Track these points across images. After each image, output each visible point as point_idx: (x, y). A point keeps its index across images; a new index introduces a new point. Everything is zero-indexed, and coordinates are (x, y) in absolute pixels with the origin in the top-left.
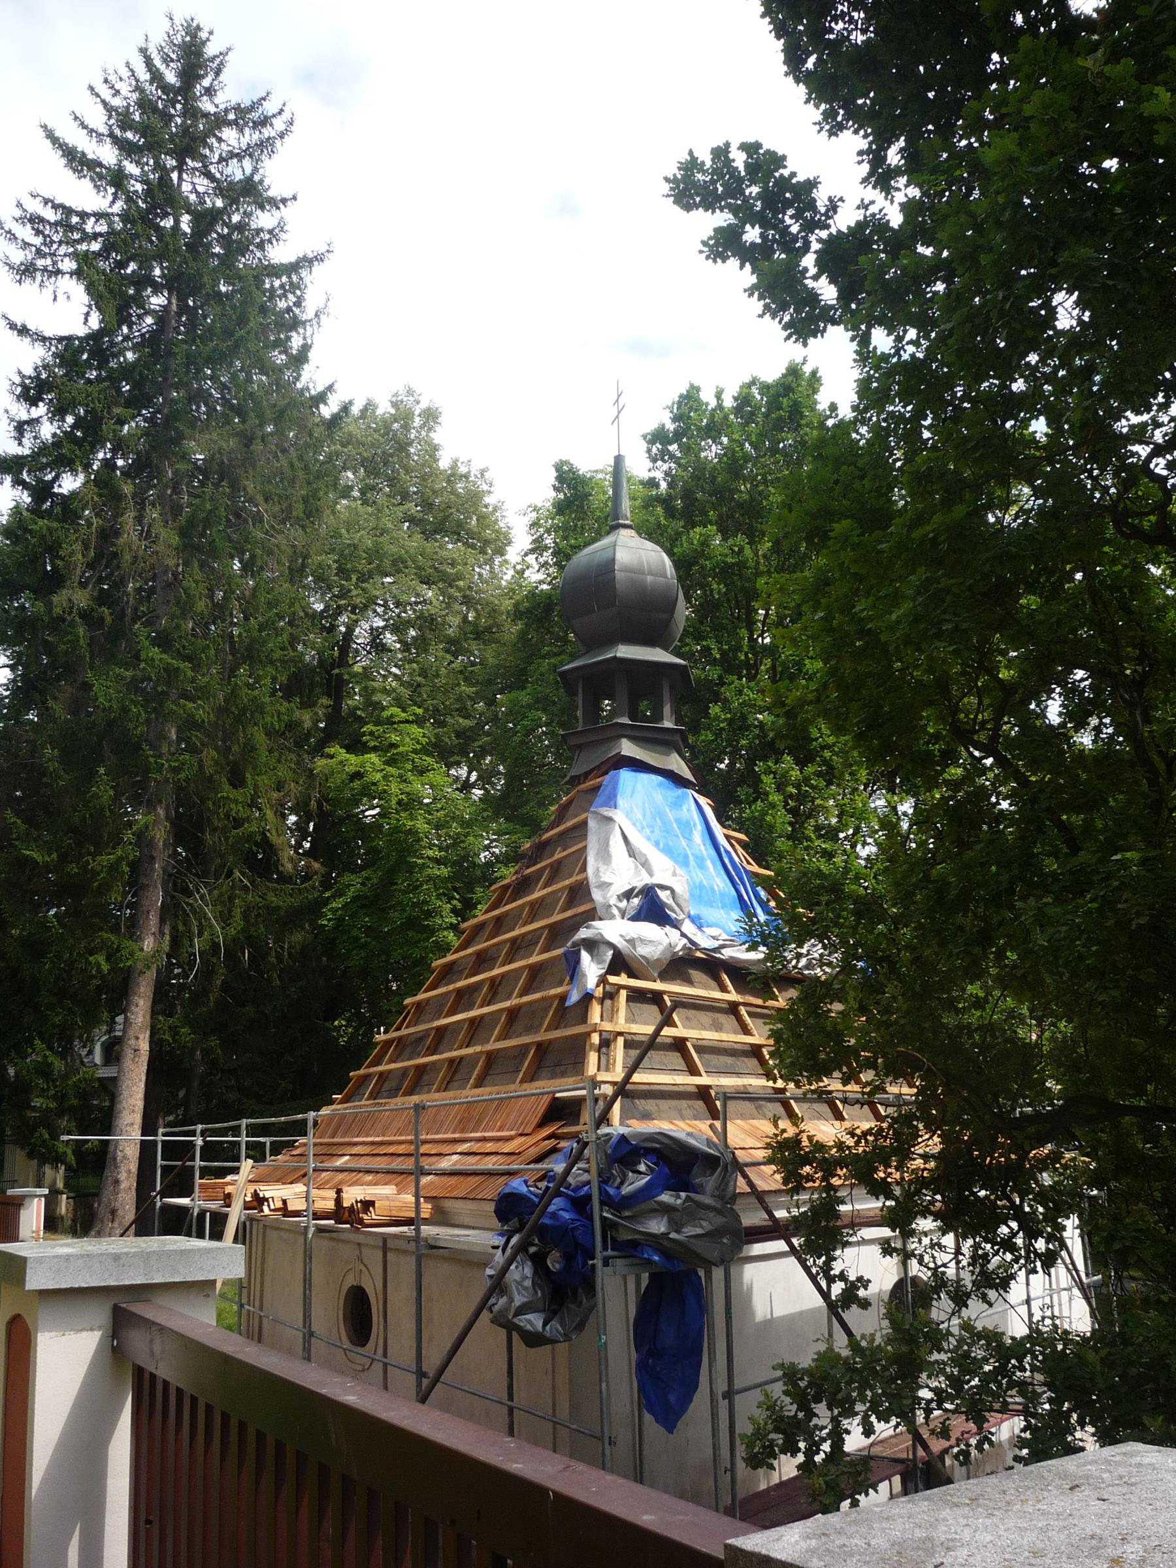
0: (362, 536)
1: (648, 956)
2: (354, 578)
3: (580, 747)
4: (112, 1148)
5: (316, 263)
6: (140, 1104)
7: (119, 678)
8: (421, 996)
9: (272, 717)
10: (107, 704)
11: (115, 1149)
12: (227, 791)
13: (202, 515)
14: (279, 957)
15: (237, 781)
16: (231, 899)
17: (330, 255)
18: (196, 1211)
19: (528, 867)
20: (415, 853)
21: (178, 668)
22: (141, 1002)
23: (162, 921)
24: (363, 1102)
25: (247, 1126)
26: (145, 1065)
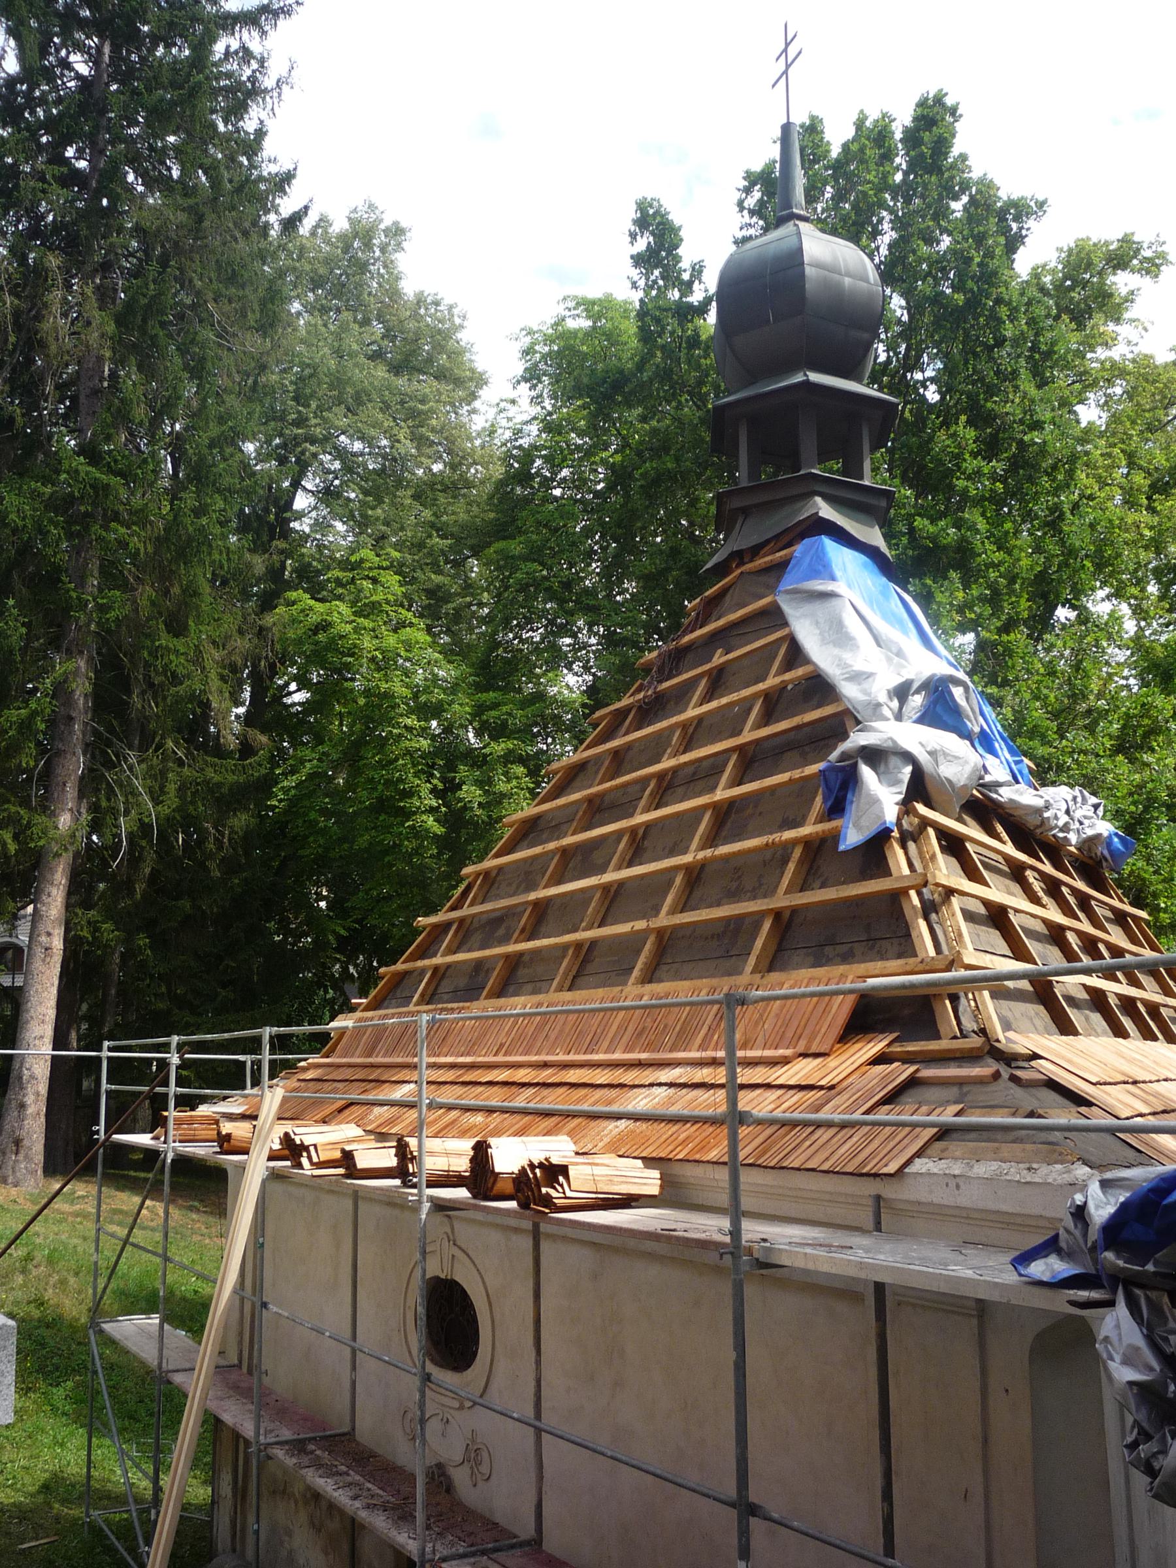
0: (324, 355)
1: (954, 780)
2: (314, 405)
3: (745, 512)
4: (16, 1065)
5: (282, 16)
6: (51, 1013)
7: (35, 495)
8: (489, 863)
9: (221, 553)
10: (20, 523)
11: (21, 1067)
12: (165, 640)
13: (144, 301)
14: (219, 842)
15: (177, 628)
16: (163, 773)
17: (299, 9)
18: (170, 1157)
19: (661, 682)
20: (390, 721)
21: (108, 485)
22: (54, 891)
23: (81, 795)
24: (412, 1008)
25: (271, 1037)
26: (58, 966)
